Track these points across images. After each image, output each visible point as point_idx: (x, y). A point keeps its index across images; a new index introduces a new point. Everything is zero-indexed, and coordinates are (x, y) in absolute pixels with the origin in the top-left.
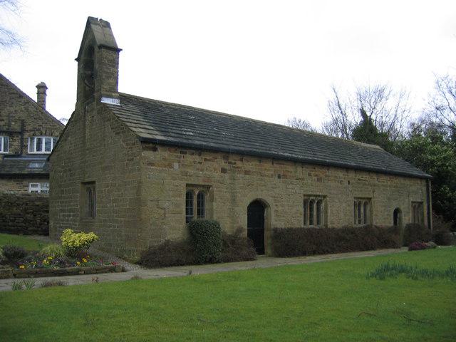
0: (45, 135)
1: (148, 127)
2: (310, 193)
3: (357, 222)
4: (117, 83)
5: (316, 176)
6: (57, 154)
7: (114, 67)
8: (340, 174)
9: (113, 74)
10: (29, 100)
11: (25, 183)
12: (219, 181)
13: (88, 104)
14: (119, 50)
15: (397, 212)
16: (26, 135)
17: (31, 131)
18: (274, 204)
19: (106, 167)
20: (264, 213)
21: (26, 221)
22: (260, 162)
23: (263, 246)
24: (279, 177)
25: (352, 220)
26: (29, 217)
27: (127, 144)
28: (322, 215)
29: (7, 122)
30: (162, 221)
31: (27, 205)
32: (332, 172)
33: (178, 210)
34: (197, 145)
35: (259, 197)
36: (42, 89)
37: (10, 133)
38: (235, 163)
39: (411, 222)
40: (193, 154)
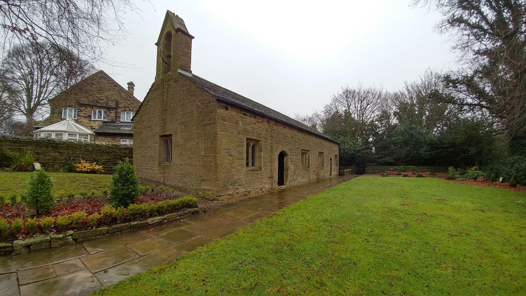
6: (139, 115)
10: (121, 89)
12: (264, 138)
19: (30, 279)
29: (106, 101)
30: (231, 166)
36: (131, 85)
37: (109, 108)
40: (250, 116)
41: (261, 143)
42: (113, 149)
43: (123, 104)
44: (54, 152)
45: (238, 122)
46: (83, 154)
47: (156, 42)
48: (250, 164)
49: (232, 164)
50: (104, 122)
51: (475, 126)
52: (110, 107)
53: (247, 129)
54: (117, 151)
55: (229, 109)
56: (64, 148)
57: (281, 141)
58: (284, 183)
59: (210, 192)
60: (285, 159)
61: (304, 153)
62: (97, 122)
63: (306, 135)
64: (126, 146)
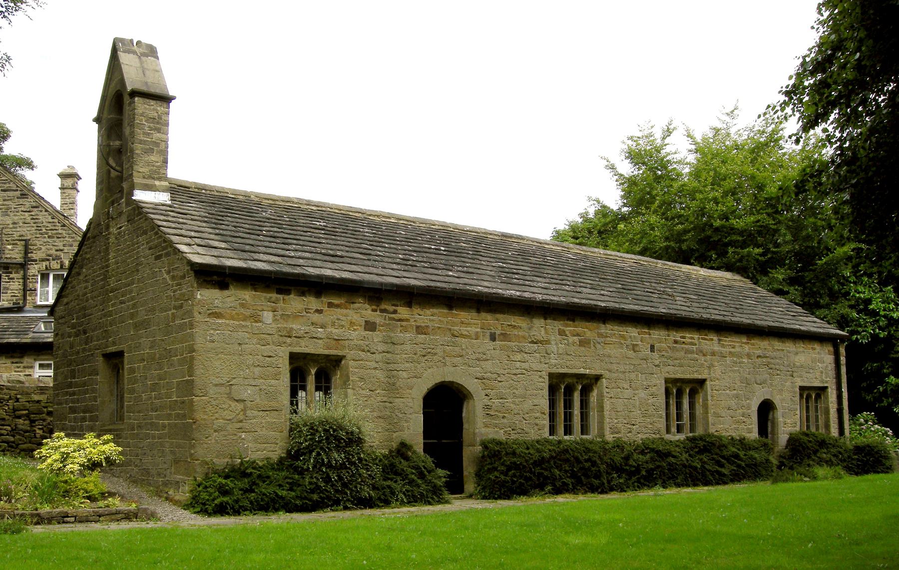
1: (216, 244)
3: (674, 429)
6: (65, 300)
7: (159, 130)
8: (633, 332)
9: (157, 144)
10: (40, 203)
11: (27, 360)
13: (113, 203)
15: (766, 409)
18: (483, 393)
21: (14, 431)
24: (493, 338)
25: (662, 425)
26: (22, 423)
27: (173, 278)
28: (593, 415)
31: (17, 400)
32: (610, 329)
33: (274, 404)
34: (310, 276)
39: (798, 428)
42: (10, 392)
43: (43, 248)
45: (260, 313)
49: (241, 421)
51: (887, 286)
52: (9, 261)
53: (292, 328)
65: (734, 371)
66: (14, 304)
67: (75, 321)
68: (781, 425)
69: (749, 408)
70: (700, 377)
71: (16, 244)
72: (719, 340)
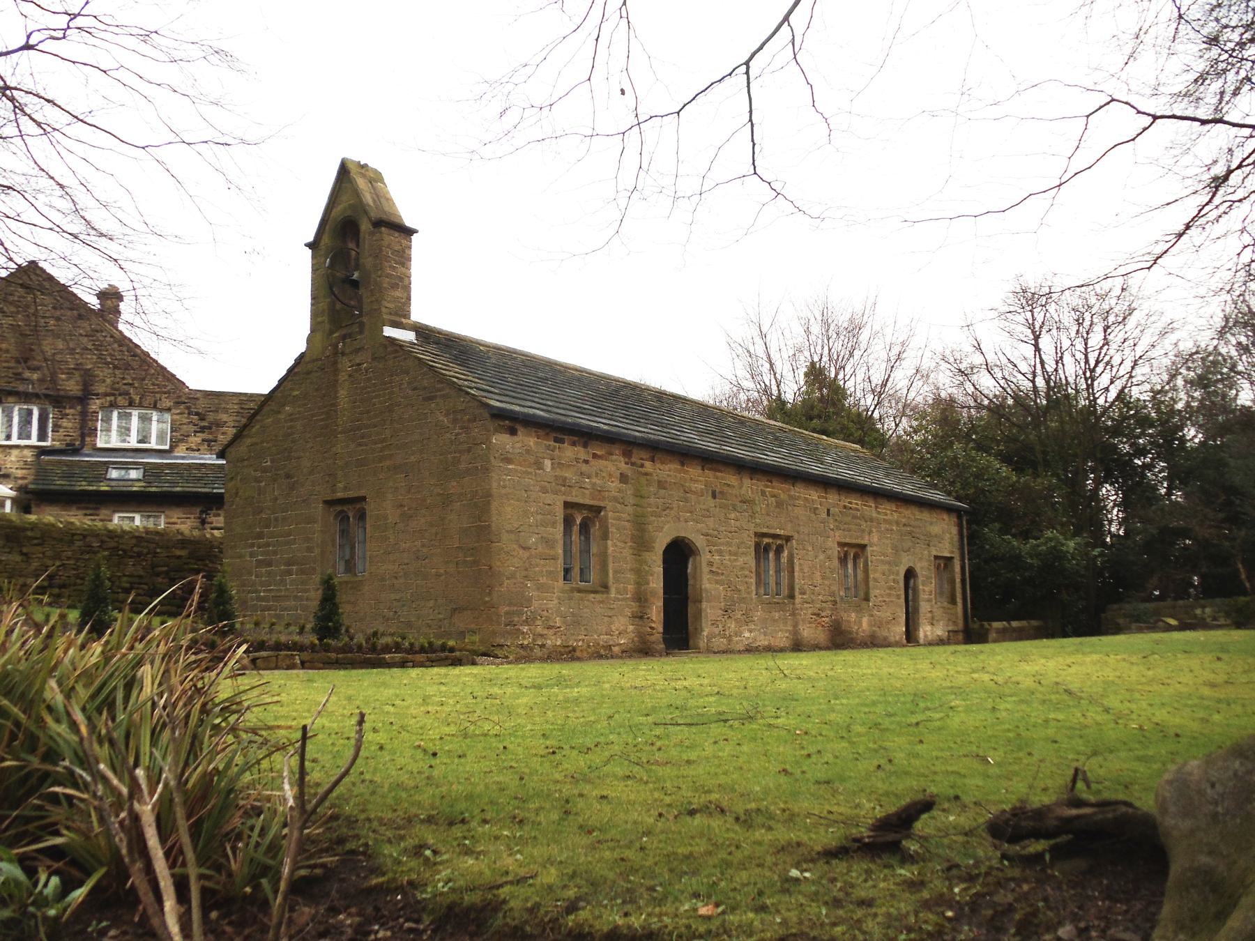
0: (140, 406)
2: (765, 530)
4: (409, 298)
5: (774, 496)
6: (248, 441)
8: (814, 495)
9: (401, 279)
12: (615, 499)
14: (410, 232)
15: (910, 574)
16: (95, 405)
17: (106, 395)
18: (707, 549)
20: (686, 568)
22: (683, 464)
23: (687, 633)
24: (714, 496)
33: (552, 553)
35: (683, 534)
36: (111, 297)
37: (58, 400)
38: (642, 466)
40: (574, 444)
41: (606, 517)
44: (9, 553)
46: (78, 560)
47: (311, 239)
48: (576, 572)
50: (42, 451)
53: (566, 478)
54: (158, 550)
55: (519, 433)
56: (36, 541)
57: (672, 509)
58: (691, 642)
59: (476, 638)
60: (690, 566)
61: (768, 545)
62: (15, 452)
63: (775, 484)
64: (182, 534)
65: (887, 538)
66: (67, 445)
67: (269, 463)
68: (921, 592)
69: (898, 574)
70: (862, 542)
71: (72, 373)
72: (876, 507)
